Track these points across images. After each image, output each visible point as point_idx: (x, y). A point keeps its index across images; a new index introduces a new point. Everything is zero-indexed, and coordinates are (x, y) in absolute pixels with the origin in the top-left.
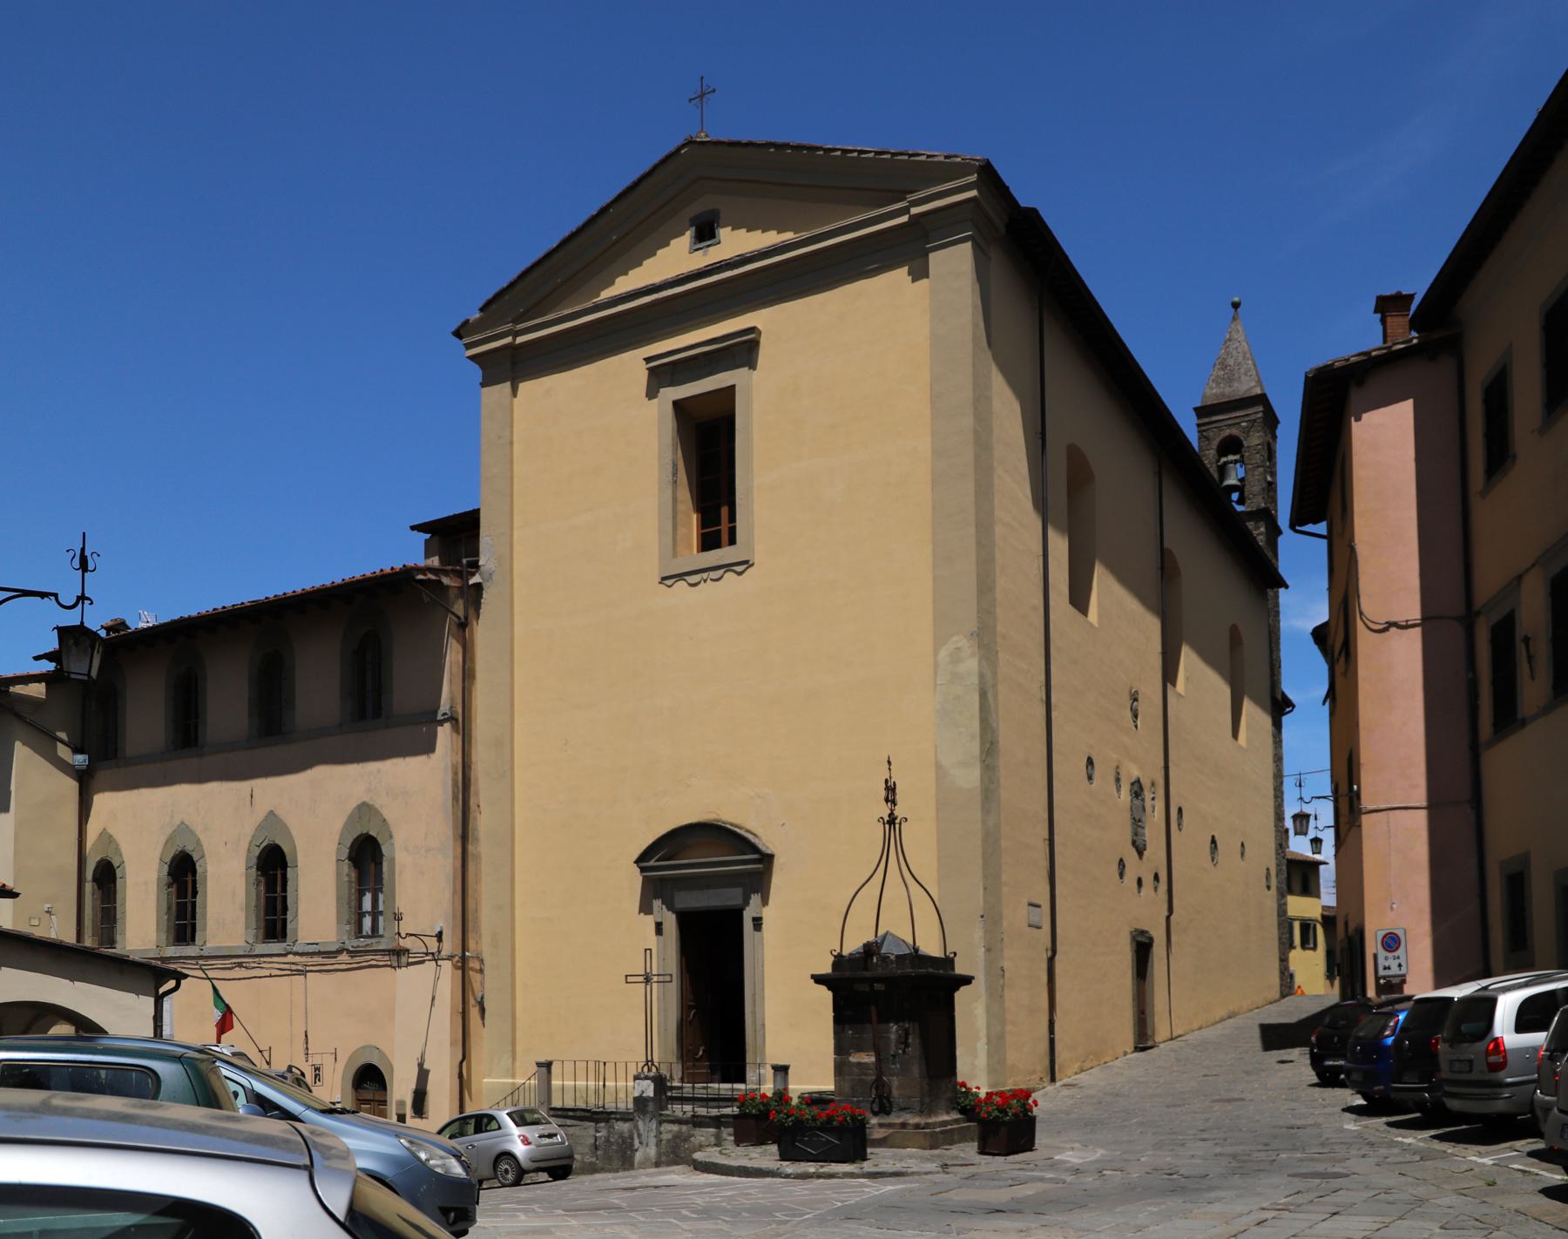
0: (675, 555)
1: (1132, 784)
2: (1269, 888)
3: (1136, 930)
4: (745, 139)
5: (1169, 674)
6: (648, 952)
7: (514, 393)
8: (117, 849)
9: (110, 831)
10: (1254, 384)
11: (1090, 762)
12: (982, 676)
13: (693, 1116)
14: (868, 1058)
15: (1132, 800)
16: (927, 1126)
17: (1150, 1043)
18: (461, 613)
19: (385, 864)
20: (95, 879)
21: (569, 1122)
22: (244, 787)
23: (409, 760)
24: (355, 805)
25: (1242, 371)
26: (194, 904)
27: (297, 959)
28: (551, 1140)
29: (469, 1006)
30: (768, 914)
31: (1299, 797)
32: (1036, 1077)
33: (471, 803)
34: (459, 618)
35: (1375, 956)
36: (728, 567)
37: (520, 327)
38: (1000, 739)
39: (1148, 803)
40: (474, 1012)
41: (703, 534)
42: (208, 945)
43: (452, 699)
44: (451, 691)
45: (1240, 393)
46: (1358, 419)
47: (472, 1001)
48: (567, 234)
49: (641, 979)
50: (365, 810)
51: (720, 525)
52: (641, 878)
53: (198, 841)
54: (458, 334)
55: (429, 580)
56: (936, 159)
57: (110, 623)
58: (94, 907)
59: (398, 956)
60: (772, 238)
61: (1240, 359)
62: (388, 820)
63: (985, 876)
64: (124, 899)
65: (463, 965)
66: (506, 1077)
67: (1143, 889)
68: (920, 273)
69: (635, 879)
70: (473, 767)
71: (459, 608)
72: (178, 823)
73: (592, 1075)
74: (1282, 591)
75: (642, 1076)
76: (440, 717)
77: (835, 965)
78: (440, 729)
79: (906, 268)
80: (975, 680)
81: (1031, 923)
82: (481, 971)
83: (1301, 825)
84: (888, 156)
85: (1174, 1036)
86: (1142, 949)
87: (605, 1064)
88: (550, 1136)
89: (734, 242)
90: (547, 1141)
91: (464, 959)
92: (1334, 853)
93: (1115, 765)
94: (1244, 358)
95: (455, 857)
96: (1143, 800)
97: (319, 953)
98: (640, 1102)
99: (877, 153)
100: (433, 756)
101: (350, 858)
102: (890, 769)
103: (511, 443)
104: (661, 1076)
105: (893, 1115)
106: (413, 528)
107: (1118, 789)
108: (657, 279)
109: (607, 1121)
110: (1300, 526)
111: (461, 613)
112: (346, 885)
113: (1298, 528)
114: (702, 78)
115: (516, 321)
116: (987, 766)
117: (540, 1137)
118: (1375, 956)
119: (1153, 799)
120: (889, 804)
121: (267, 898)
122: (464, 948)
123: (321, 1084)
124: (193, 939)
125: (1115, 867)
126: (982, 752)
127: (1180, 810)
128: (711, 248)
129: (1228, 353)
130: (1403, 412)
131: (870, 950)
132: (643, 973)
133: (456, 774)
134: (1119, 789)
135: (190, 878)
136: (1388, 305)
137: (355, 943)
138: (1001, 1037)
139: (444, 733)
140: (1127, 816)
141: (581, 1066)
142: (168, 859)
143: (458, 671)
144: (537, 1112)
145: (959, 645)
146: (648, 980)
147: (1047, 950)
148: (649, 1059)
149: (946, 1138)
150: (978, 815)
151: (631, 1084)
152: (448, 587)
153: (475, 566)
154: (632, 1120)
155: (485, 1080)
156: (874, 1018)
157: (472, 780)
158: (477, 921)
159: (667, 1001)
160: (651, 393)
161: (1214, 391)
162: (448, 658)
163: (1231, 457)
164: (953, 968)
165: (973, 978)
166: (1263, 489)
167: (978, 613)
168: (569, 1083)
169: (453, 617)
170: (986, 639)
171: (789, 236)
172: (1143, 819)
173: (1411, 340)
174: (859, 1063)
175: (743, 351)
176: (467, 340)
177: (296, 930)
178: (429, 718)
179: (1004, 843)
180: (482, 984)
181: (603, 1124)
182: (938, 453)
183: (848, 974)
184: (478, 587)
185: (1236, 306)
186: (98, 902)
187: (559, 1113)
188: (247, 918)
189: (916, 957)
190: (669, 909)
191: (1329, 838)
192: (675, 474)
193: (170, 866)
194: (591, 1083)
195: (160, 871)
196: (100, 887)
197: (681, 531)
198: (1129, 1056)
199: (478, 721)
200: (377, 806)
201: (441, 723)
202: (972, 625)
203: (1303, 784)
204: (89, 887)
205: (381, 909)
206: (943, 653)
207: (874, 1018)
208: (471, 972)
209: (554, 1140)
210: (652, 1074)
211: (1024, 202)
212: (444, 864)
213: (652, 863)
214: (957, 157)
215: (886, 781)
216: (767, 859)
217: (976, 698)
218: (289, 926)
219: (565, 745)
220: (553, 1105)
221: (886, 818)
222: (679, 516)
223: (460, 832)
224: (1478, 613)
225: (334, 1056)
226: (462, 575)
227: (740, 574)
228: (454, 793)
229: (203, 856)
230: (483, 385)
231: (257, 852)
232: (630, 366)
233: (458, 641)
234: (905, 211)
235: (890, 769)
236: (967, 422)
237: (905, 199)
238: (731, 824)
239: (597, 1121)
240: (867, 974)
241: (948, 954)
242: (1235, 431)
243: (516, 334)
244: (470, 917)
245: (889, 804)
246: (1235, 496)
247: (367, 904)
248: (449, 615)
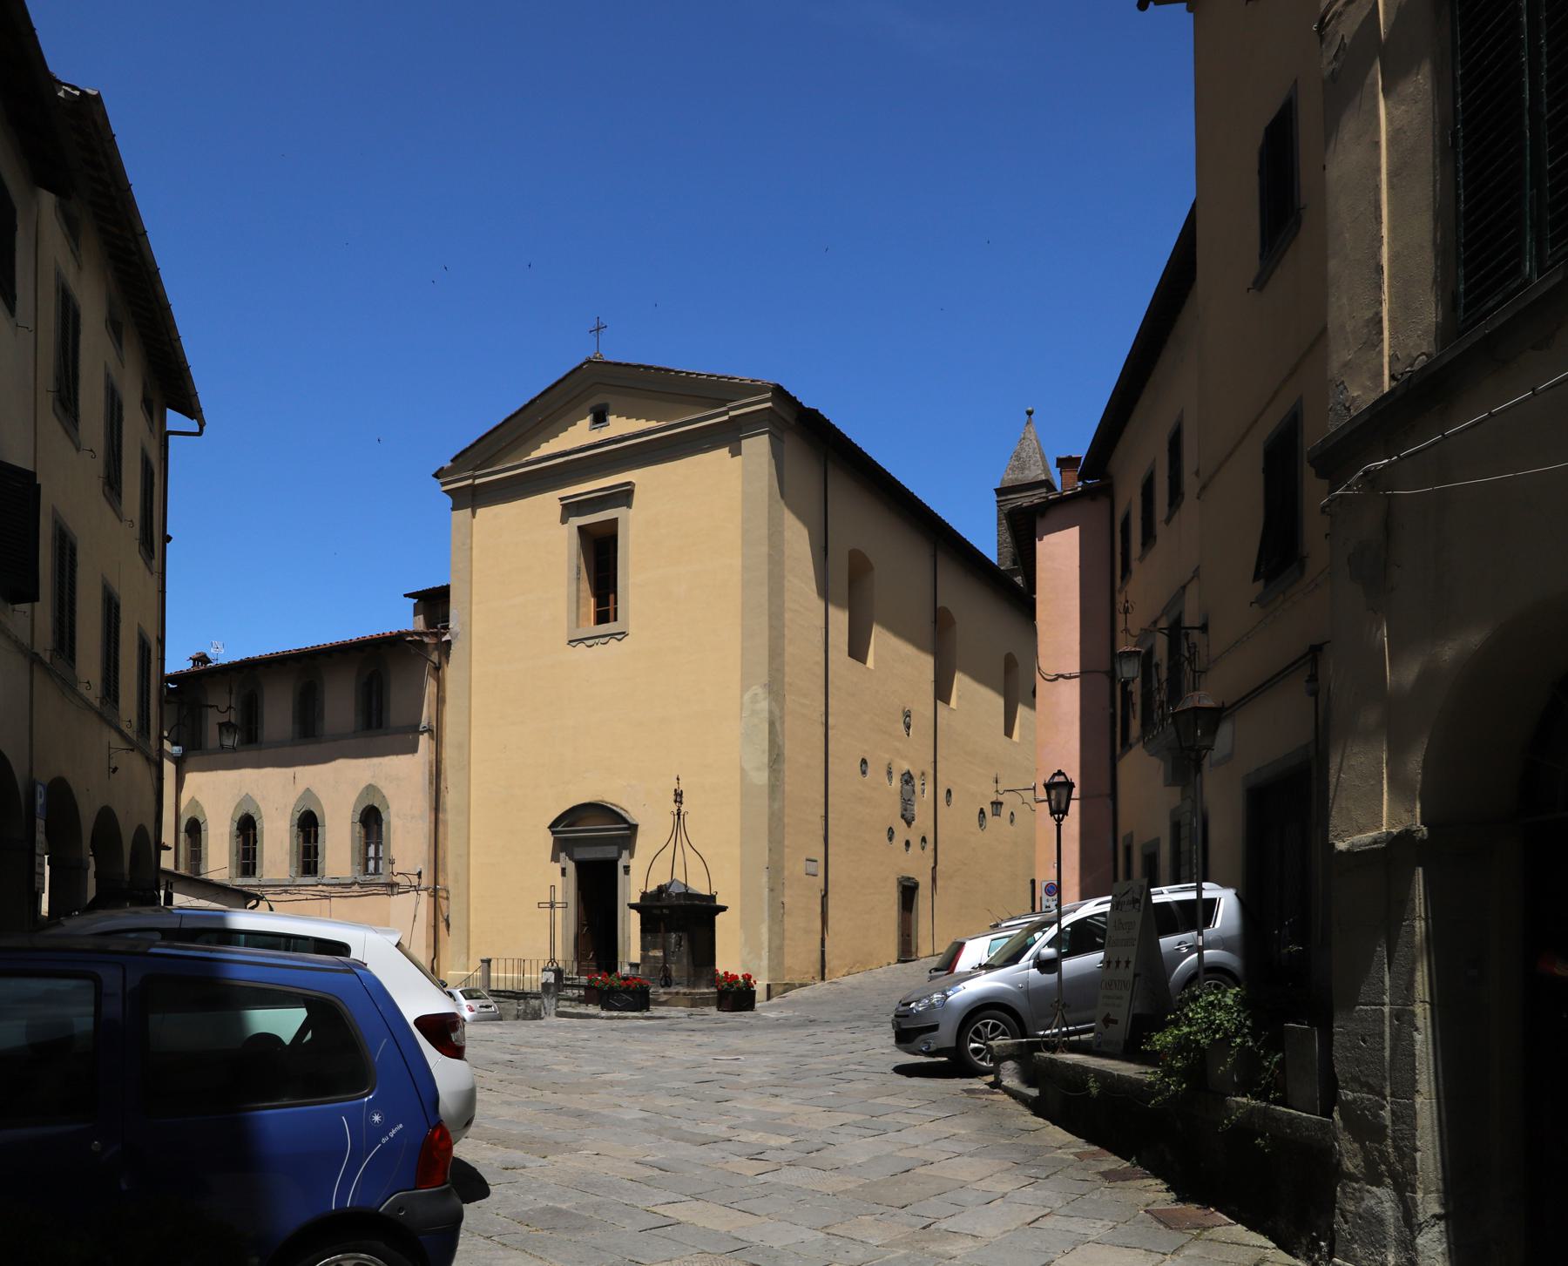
0: (578, 626)
1: (903, 775)
4: (624, 362)
5: (942, 692)
7: (474, 515)
8: (202, 810)
9: (197, 798)
10: (1040, 472)
11: (864, 762)
12: (771, 712)
13: (579, 996)
14: (659, 953)
15: (902, 787)
16: (690, 994)
17: (914, 957)
18: (436, 661)
19: (384, 826)
20: (186, 831)
21: (501, 1000)
22: (289, 771)
23: (401, 757)
24: (364, 786)
26: (254, 850)
27: (325, 888)
28: (487, 1010)
29: (439, 922)
30: (633, 863)
31: (995, 790)
32: (809, 976)
33: (442, 786)
34: (435, 664)
35: (1041, 898)
36: (612, 635)
37: (478, 473)
38: (786, 752)
39: (918, 788)
40: (442, 926)
41: (598, 612)
42: (264, 877)
43: (430, 717)
44: (429, 712)
45: (1030, 478)
46: (1041, 539)
47: (441, 919)
48: (508, 415)
50: (371, 789)
51: (608, 605)
52: (552, 839)
53: (258, 806)
54: (436, 476)
55: (415, 640)
56: (745, 382)
57: (196, 656)
58: (186, 849)
59: (392, 887)
60: (642, 425)
62: (387, 797)
63: (770, 841)
64: (207, 845)
65: (435, 894)
66: (463, 970)
67: (910, 849)
68: (736, 452)
69: (549, 839)
70: (443, 762)
71: (435, 657)
72: (244, 794)
73: (516, 971)
76: (421, 729)
77: (642, 898)
78: (421, 737)
79: (727, 449)
80: (766, 715)
81: (808, 872)
82: (447, 898)
83: (997, 809)
84: (715, 378)
85: (936, 953)
86: (908, 892)
88: (487, 1007)
89: (618, 426)
90: (485, 1010)
91: (435, 890)
93: (887, 763)
94: (1034, 452)
95: (430, 822)
96: (913, 786)
97: (339, 885)
98: (546, 985)
99: (708, 376)
100: (416, 755)
101: (361, 821)
103: (471, 548)
104: (559, 969)
105: (672, 988)
106: (406, 596)
108: (568, 447)
109: (525, 999)
111: (436, 661)
112: (358, 839)
115: (475, 469)
116: (774, 770)
117: (481, 1007)
118: (1041, 898)
119: (923, 784)
121: (304, 847)
122: (436, 883)
124: (254, 873)
125: (885, 835)
126: (769, 761)
127: (949, 792)
128: (603, 428)
129: (1022, 449)
130: (1073, 534)
131: (661, 889)
132: (549, 901)
133: (432, 767)
134: (890, 779)
135: (251, 832)
137: (363, 878)
138: (781, 948)
139: (424, 740)
140: (898, 798)
141: (509, 963)
142: (237, 819)
143: (434, 698)
144: (480, 992)
145: (756, 692)
146: (552, 906)
149: (701, 1002)
150: (766, 802)
152: (427, 644)
153: (446, 628)
154: (540, 998)
155: (449, 972)
156: (662, 929)
157: (443, 771)
158: (444, 864)
159: (565, 922)
160: (564, 521)
162: (427, 691)
164: (715, 901)
165: (727, 907)
167: (769, 671)
168: (509, 975)
169: (431, 664)
170: (775, 688)
171: (653, 424)
172: (913, 798)
173: (1077, 488)
175: (623, 496)
176: (442, 480)
178: (415, 730)
179: (786, 820)
180: (448, 907)
181: (522, 1001)
182: (745, 568)
183: (648, 904)
184: (449, 643)
185: (1030, 413)
186: (189, 846)
187: (495, 993)
188: (291, 860)
189: (689, 895)
190: (570, 859)
192: (578, 573)
193: (238, 823)
194: (516, 975)
195: (231, 826)
196: (190, 836)
197: (583, 610)
198: (892, 966)
199: (447, 731)
200: (379, 787)
201: (422, 733)
202: (765, 679)
204: (182, 836)
205: (381, 856)
206: (747, 697)
207: (662, 929)
208: (440, 899)
209: (489, 1010)
210: (553, 968)
211: (806, 405)
212: (424, 827)
213: (559, 829)
214: (758, 381)
215: (676, 790)
216: (633, 828)
217: (766, 726)
218: (319, 866)
219: (505, 748)
220: (491, 988)
221: (676, 812)
222: (581, 601)
226: (438, 635)
227: (619, 640)
228: (430, 779)
229: (261, 818)
230: (453, 509)
231: (298, 815)
232: (549, 503)
233: (434, 679)
234: (726, 413)
236: (765, 549)
237: (725, 406)
238: (612, 804)
239: (518, 999)
240: (658, 904)
243: (475, 478)
244: (440, 862)
247: (372, 852)
248: (429, 662)
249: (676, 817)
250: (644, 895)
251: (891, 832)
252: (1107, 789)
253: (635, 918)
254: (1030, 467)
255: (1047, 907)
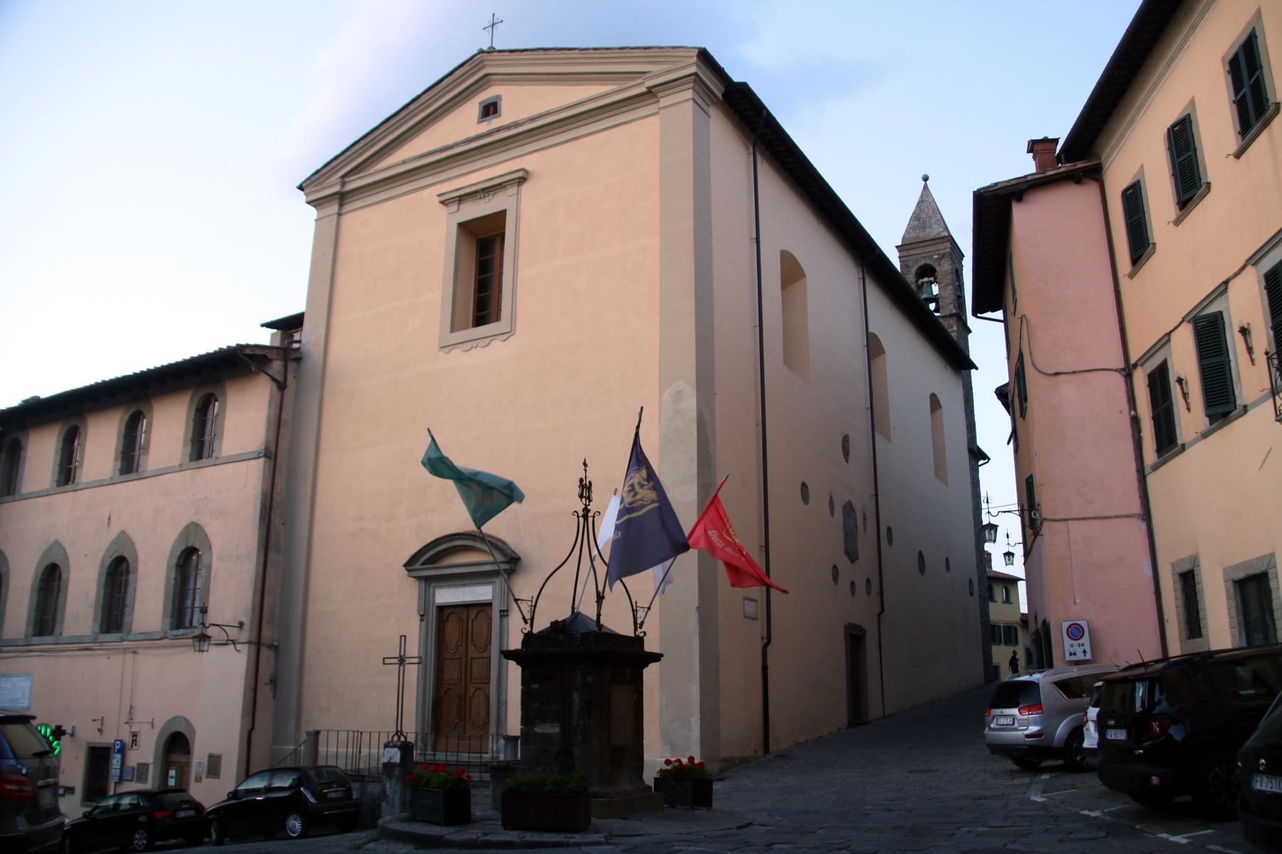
2: (972, 594)
3: (849, 624)
6: (403, 638)
10: (942, 229)
14: (553, 729)
25: (932, 221)
41: (477, 317)
42: (64, 635)
49: (396, 661)
53: (66, 554)
61: (930, 214)
74: (973, 371)
75: (391, 744)
77: (524, 642)
87: (361, 733)
92: (1023, 561)
98: (388, 766)
102: (586, 471)
106: (263, 325)
107: (832, 509)
110: (980, 313)
113: (979, 315)
114: (494, 15)
120: (584, 500)
123: (137, 748)
132: (398, 656)
136: (1038, 147)
146: (402, 660)
147: (762, 638)
148: (399, 729)
151: (381, 750)
161: (912, 235)
163: (926, 279)
166: (954, 300)
174: (544, 735)
177: (131, 623)
191: (1019, 551)
203: (989, 501)
207: (56, 821)
211: (736, 78)
215: (581, 480)
221: (581, 513)
223: (264, 543)
224: (1135, 366)
225: (151, 725)
235: (586, 471)
241: (637, 633)
242: (929, 262)
245: (584, 500)
246: (932, 306)
249: (582, 520)
250: (529, 638)
251: (835, 571)
252: (1136, 508)
253: (514, 672)
254: (931, 225)
255: (1071, 654)
